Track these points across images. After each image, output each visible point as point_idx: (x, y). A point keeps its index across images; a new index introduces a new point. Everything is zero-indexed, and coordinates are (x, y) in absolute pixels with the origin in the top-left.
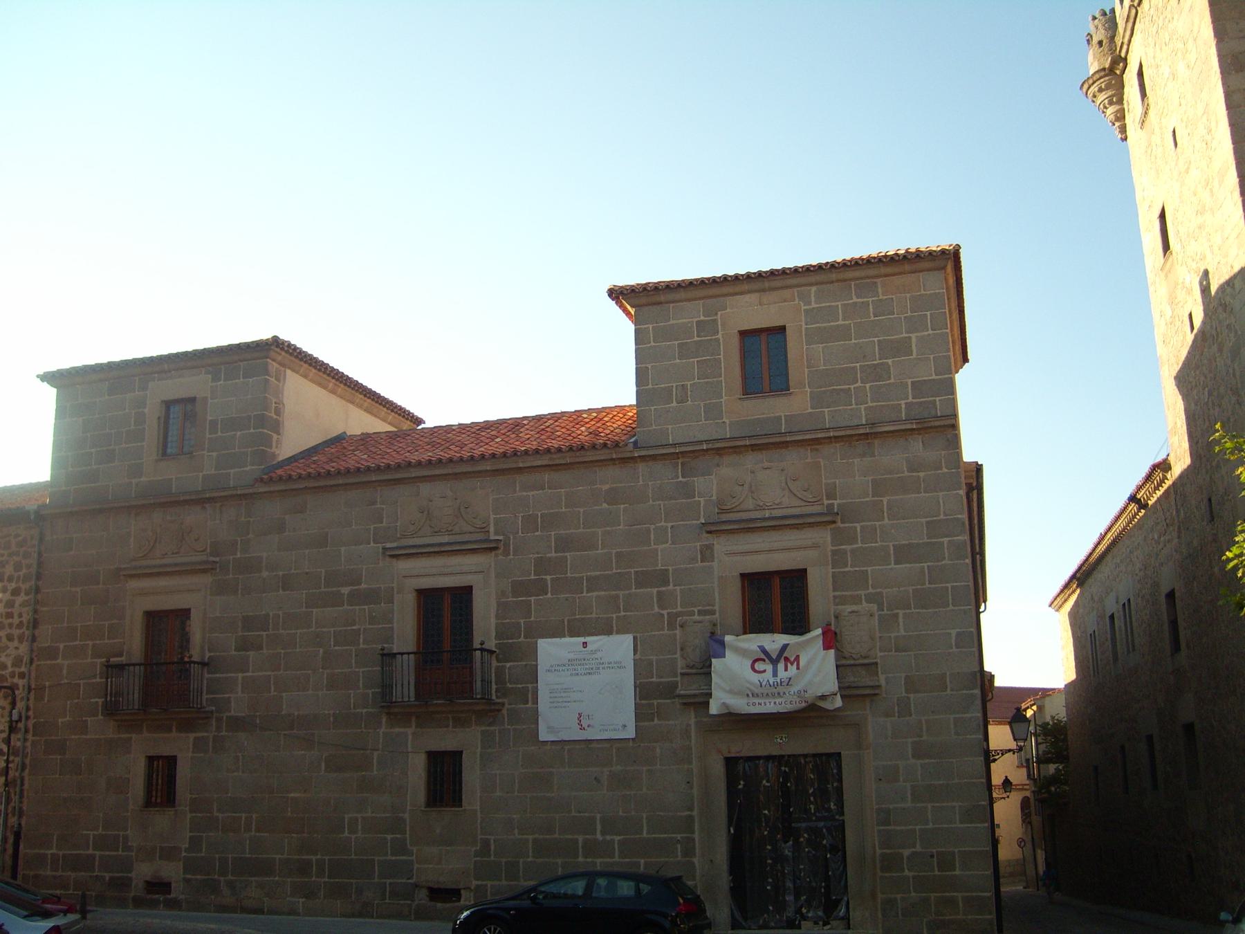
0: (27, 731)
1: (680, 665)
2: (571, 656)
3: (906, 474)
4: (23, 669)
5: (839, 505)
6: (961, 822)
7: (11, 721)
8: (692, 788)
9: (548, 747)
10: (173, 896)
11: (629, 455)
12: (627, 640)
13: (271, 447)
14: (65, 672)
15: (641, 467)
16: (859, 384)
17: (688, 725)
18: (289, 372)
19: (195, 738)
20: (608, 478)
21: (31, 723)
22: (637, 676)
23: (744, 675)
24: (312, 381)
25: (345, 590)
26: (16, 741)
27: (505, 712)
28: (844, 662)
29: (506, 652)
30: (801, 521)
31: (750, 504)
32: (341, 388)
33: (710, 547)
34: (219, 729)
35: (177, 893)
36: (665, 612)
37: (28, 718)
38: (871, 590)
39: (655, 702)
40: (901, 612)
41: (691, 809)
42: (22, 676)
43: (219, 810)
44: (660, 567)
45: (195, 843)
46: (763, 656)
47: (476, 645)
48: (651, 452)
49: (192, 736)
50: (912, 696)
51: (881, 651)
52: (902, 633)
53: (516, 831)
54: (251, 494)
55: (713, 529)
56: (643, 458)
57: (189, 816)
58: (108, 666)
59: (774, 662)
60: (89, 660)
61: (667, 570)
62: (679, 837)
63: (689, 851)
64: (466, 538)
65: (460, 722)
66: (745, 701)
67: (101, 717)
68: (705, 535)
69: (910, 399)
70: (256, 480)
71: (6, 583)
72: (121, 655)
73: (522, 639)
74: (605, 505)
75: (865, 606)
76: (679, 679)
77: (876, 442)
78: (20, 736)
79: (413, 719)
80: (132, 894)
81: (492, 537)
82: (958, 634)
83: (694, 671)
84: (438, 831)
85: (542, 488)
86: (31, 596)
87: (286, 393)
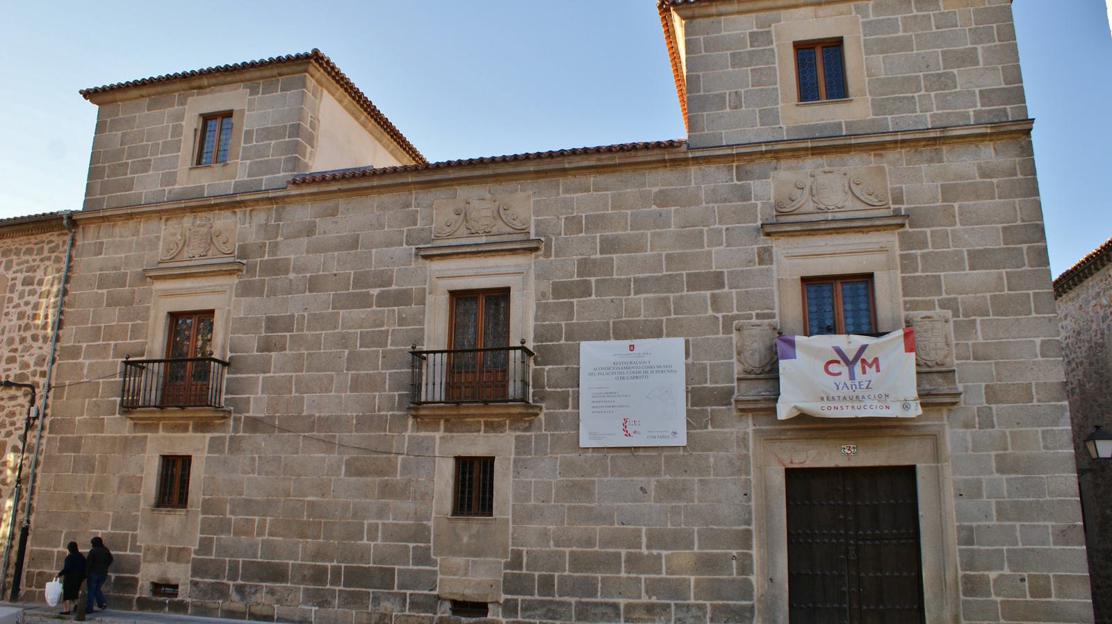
0: (43, 428)
1: (737, 370)
2: (617, 359)
3: (978, 179)
4: (45, 368)
5: (906, 209)
6: (1055, 544)
7: (29, 418)
8: (749, 500)
9: (589, 454)
10: (179, 598)
11: (682, 156)
12: (679, 342)
13: (304, 156)
14: (85, 371)
15: (693, 170)
16: (923, 92)
17: (746, 433)
18: (325, 92)
19: (211, 439)
20: (658, 181)
21: (47, 421)
22: (689, 381)
23: (811, 378)
24: (345, 108)
25: (375, 292)
26: (32, 438)
27: (542, 416)
28: (922, 370)
29: (542, 355)
30: (868, 223)
31: (810, 207)
32: (372, 123)
33: (767, 250)
34: (236, 429)
35: (184, 594)
36: (720, 315)
37: (45, 415)
38: (944, 296)
39: (709, 408)
40: (978, 319)
41: (748, 522)
42: (43, 374)
43: (232, 512)
44: (714, 269)
45: (205, 546)
46: (838, 358)
47: (514, 342)
48: (706, 153)
49: (208, 436)
50: (994, 406)
51: (958, 359)
52: (981, 340)
53: (552, 543)
54: (283, 197)
55: (768, 230)
56: (696, 160)
57: (201, 516)
58: (127, 363)
59: (850, 364)
60: (110, 360)
61: (722, 273)
62: (734, 552)
63: (745, 568)
64: (506, 238)
65: (491, 427)
66: (820, 404)
67: (117, 416)
68: (763, 237)
69: (979, 107)
70: (288, 182)
71: (35, 286)
72: (143, 355)
73: (563, 342)
74: (654, 207)
75: (938, 312)
76: (735, 384)
77: (944, 148)
78: (36, 433)
79: (442, 422)
80: (137, 596)
81: (532, 237)
82: (1043, 343)
83: (753, 376)
84: (465, 540)
85: (588, 190)
86: (59, 298)
87: (321, 111)
